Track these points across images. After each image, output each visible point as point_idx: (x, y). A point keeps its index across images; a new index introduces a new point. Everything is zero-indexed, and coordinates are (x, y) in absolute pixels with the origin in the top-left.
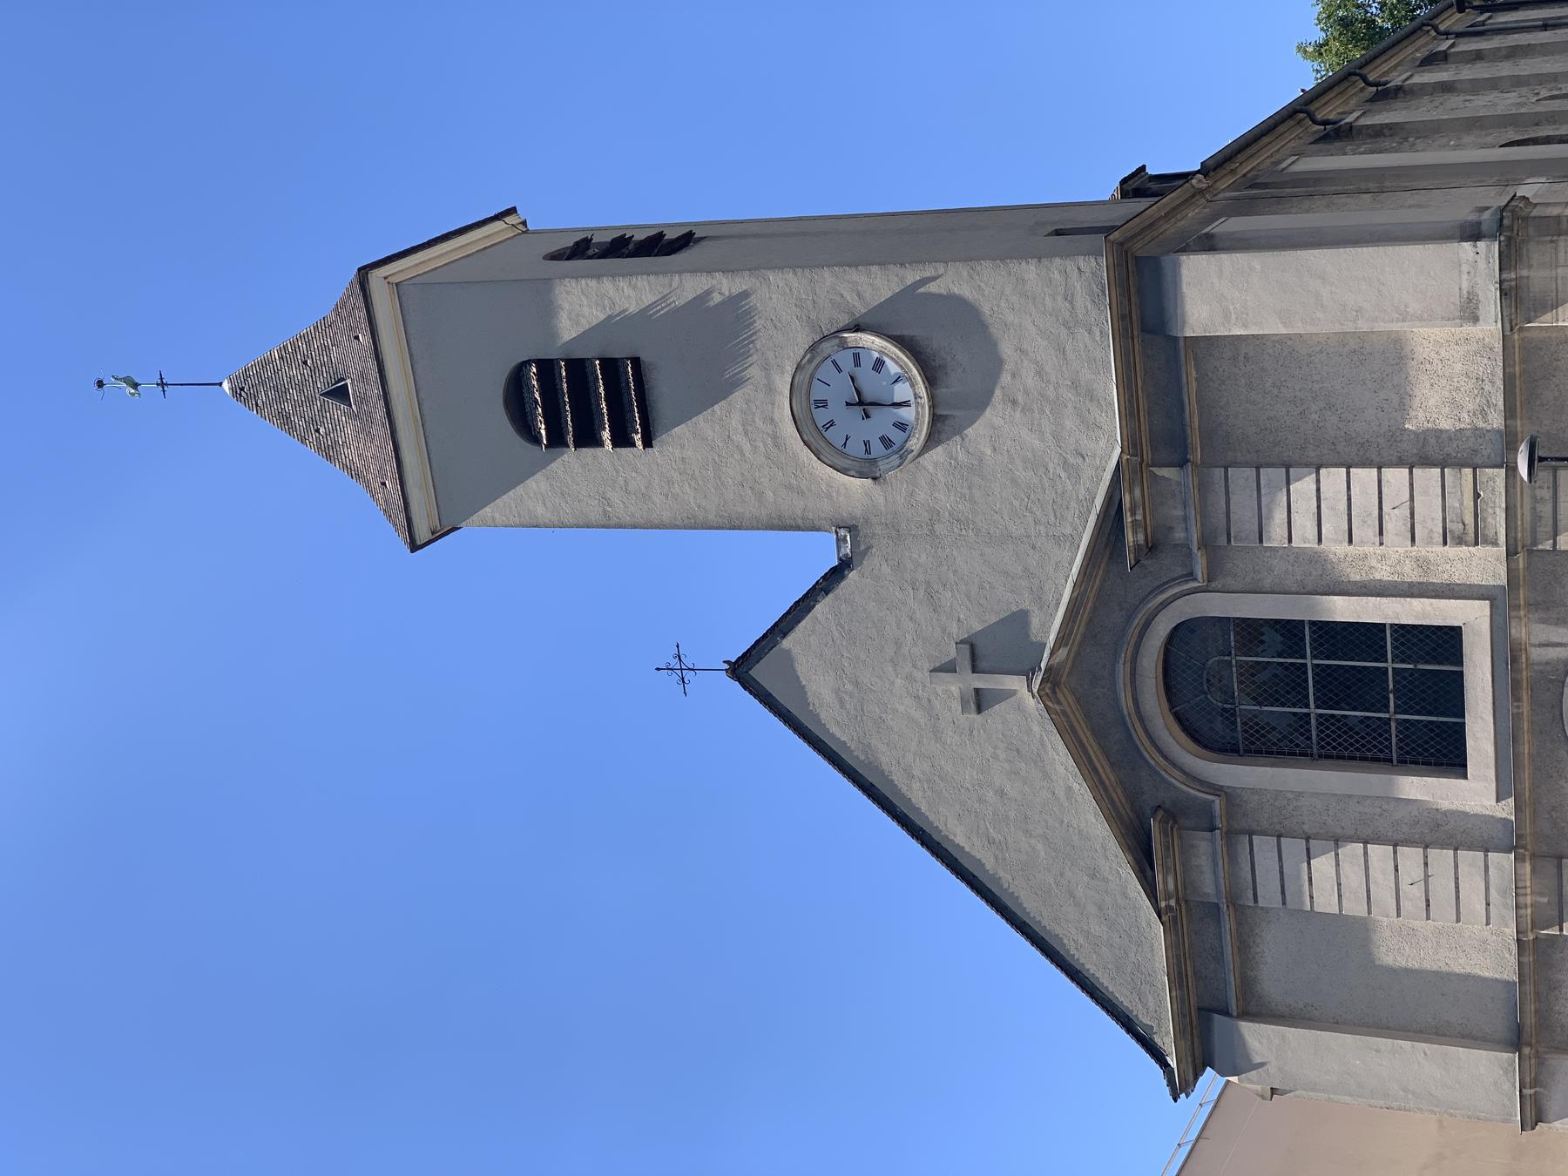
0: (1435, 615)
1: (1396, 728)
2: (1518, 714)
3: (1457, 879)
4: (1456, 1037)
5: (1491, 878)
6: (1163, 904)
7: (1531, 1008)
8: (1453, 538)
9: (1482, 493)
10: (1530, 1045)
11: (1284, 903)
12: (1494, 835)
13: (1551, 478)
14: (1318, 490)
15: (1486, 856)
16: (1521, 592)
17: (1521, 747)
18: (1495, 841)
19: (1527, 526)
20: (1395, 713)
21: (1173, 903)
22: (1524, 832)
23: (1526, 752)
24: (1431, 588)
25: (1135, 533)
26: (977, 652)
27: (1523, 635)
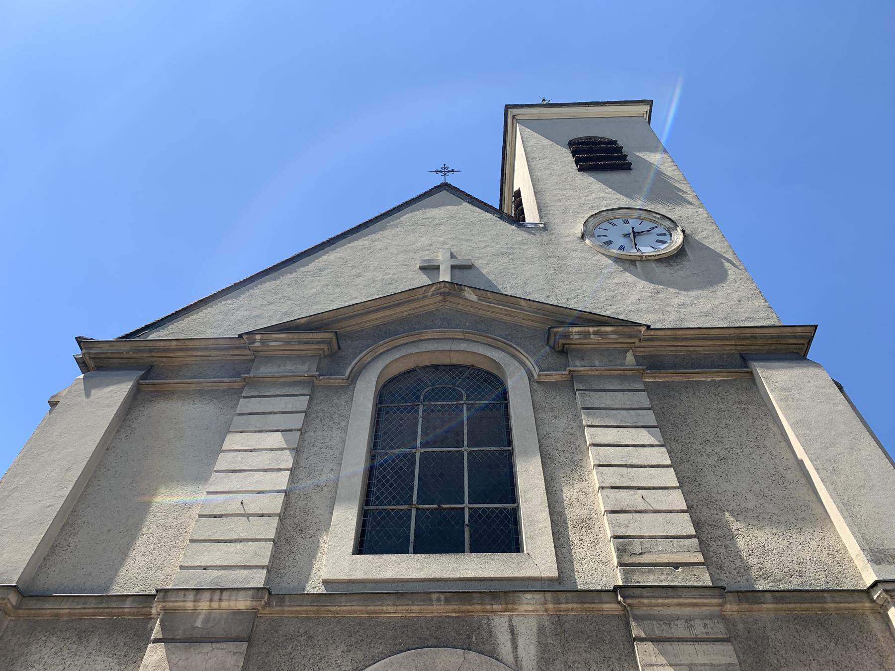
0: (535, 530)
1: (401, 510)
2: (431, 600)
3: (241, 541)
4: (56, 541)
5: (237, 571)
6: (258, 337)
7: (65, 609)
8: (624, 545)
9: (680, 570)
10: (17, 607)
11: (239, 414)
12: (284, 579)
13: (720, 636)
14: (643, 446)
15: (263, 567)
16: (575, 606)
17: (390, 603)
18: (278, 579)
19: (657, 611)
20: (417, 509)
21: (257, 344)
22: (287, 603)
23: (384, 608)
24: (561, 529)
25: (579, 333)
26: (465, 270)
27: (526, 607)
